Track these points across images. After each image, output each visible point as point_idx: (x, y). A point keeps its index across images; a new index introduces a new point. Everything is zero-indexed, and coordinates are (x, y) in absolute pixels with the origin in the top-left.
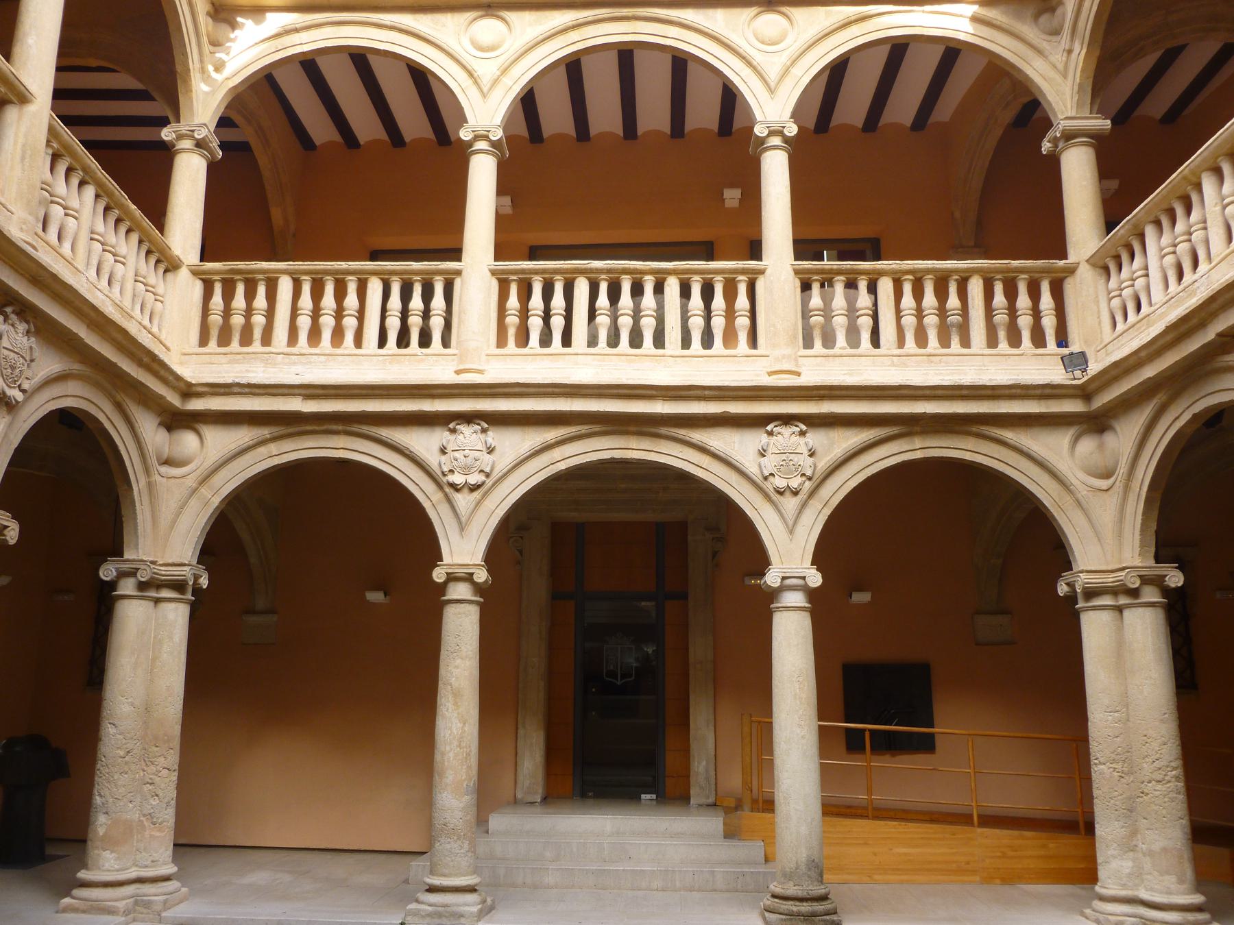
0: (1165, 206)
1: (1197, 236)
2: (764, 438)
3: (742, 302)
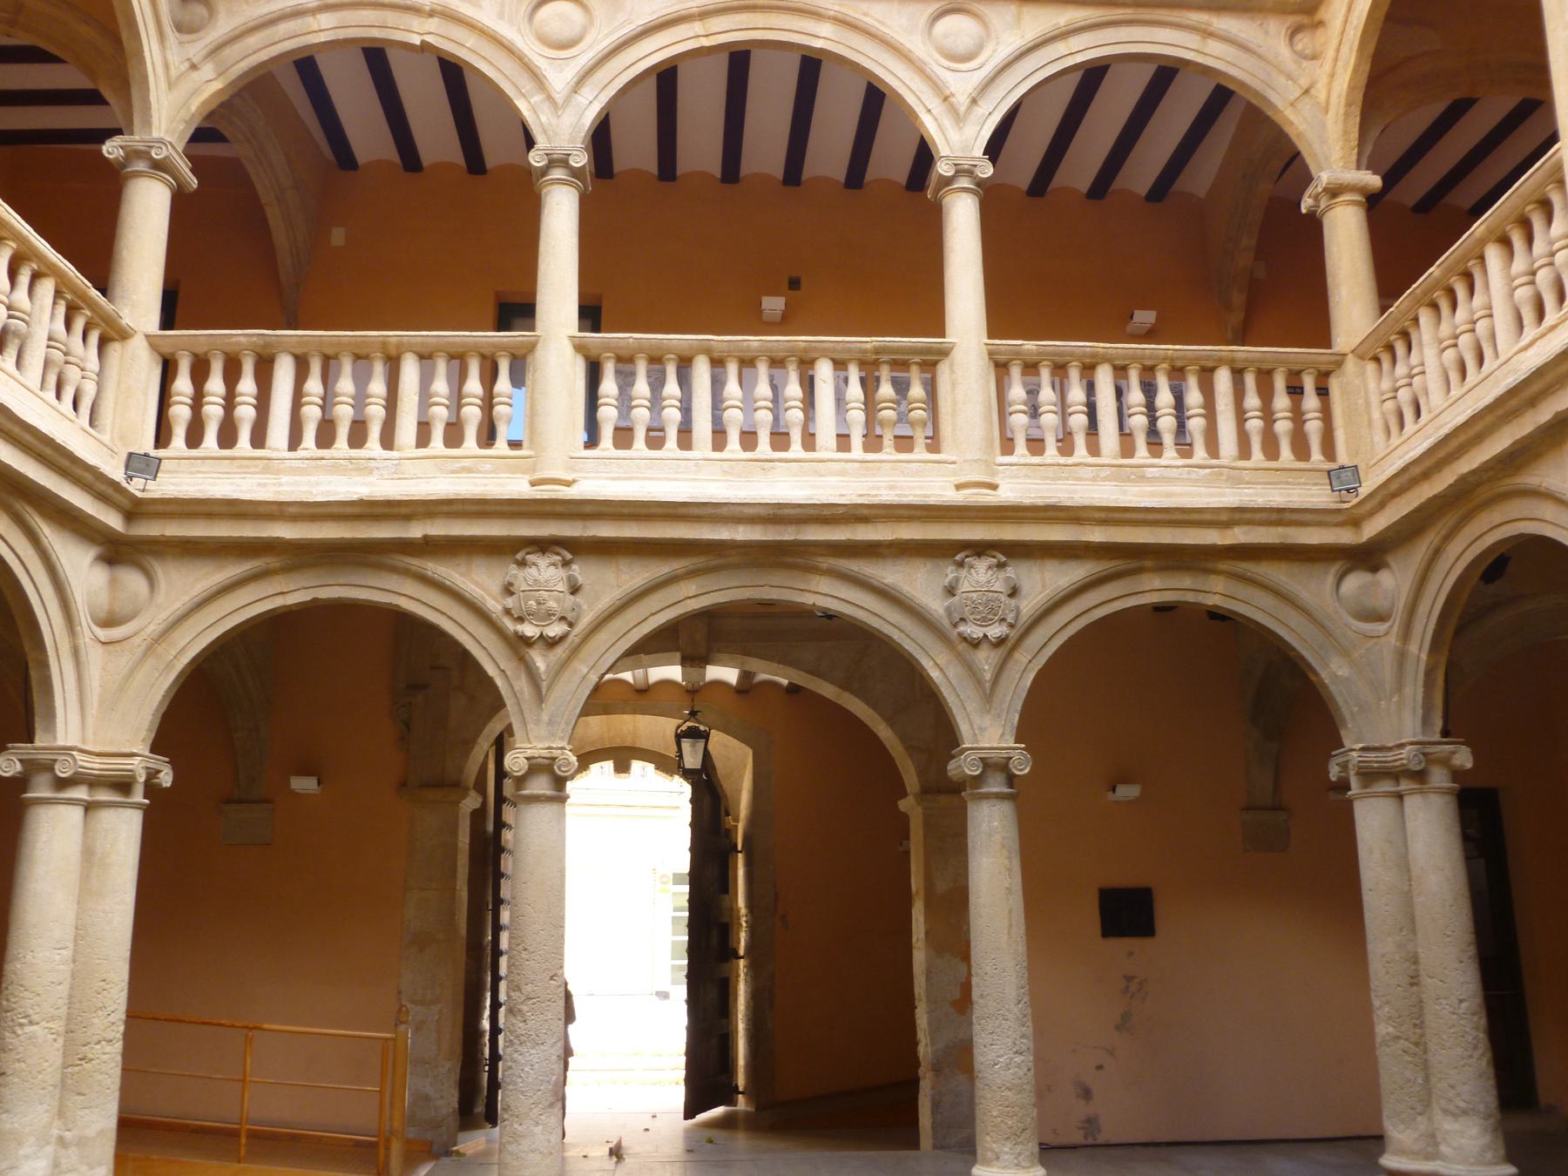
0: (1461, 268)
1: (1481, 327)
3: (1311, 402)
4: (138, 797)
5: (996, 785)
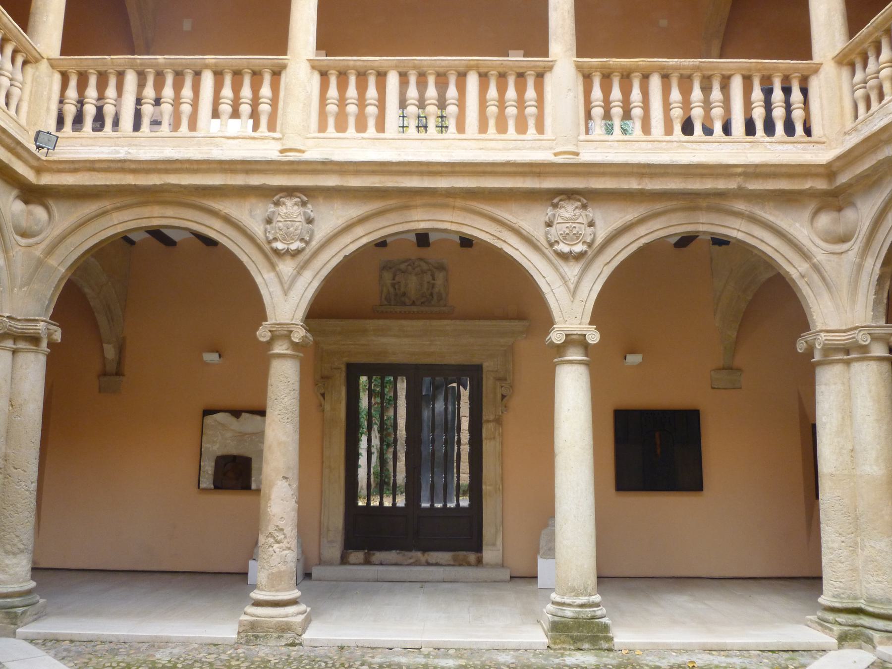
3: (796, 96)
4: (44, 344)
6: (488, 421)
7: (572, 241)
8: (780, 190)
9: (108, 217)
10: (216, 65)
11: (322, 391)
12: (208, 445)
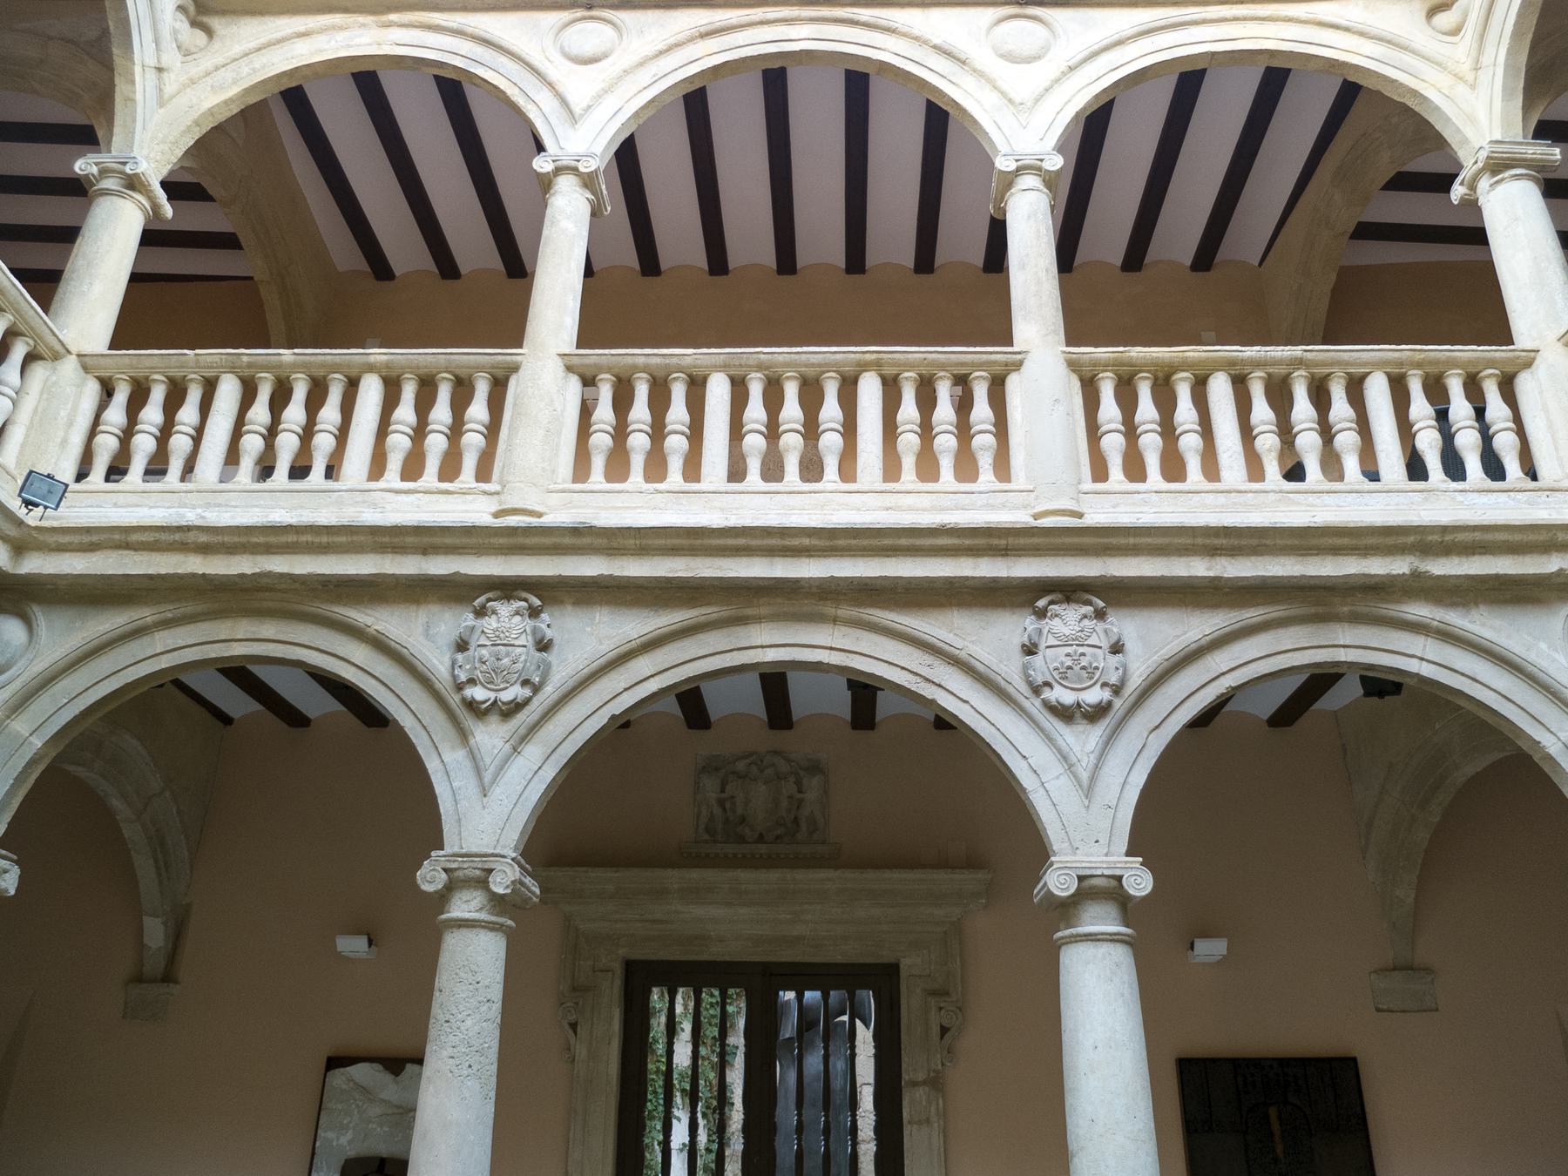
2: (1030, 622)
3: (982, 411)
5: (1101, 920)
6: (915, 1084)
7: (1080, 680)
8: (1497, 577)
9: (145, 640)
10: (388, 366)
11: (572, 1018)
12: (330, 1135)
